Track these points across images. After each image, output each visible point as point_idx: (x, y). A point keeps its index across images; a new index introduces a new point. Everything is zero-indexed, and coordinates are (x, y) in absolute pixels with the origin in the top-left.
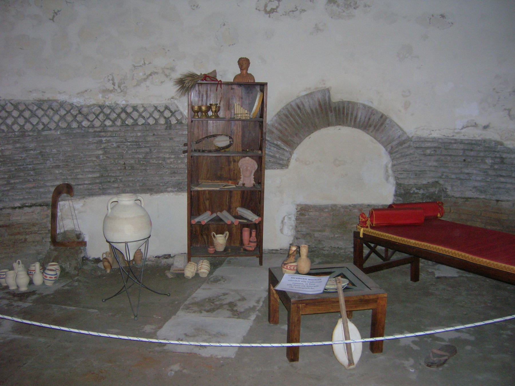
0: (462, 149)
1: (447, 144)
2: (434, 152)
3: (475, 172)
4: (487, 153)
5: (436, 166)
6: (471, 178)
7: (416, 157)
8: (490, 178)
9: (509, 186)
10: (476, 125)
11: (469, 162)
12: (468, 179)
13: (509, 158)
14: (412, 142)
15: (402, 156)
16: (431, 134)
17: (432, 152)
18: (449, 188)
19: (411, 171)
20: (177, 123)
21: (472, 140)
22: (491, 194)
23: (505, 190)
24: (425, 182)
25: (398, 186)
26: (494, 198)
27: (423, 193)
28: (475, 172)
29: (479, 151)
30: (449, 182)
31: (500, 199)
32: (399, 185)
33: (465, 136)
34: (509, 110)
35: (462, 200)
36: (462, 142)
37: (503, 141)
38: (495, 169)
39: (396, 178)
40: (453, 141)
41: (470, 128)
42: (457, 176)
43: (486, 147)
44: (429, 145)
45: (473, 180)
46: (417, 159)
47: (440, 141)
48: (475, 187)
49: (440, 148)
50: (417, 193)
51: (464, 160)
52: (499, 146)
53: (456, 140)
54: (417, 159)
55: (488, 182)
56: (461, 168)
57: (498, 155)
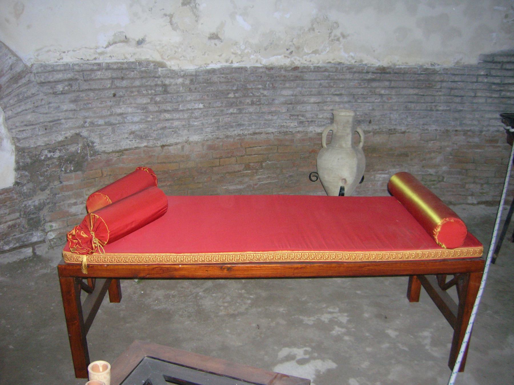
0: (110, 79)
1: (88, 73)
2: (69, 87)
3: (130, 110)
4: (144, 81)
5: (75, 110)
6: (126, 120)
7: (42, 100)
8: (151, 117)
9: (176, 123)
10: (126, 40)
11: (121, 97)
12: (122, 123)
13: (174, 85)
14: (32, 75)
15: (20, 101)
16: (62, 59)
17: (66, 88)
18: (97, 140)
19: (36, 124)
20: (234, 97)
21: (123, 63)
22: (155, 139)
23: (171, 130)
24: (61, 138)
25: (20, 153)
26: (159, 143)
27: (60, 157)
28: (130, 110)
29: (132, 79)
30: (96, 132)
31: (167, 144)
32: (20, 151)
33: (113, 58)
34: (171, 16)
35: (117, 154)
36: (108, 67)
37: (165, 61)
38: (156, 103)
39: (16, 140)
40: (95, 68)
41: (118, 45)
42: (107, 120)
43: (142, 72)
44: (59, 76)
45: (129, 123)
46: (43, 103)
47: (77, 68)
48: (132, 133)
49: (76, 79)
50: (51, 158)
51: (114, 95)
52: (160, 69)
53: (99, 64)
54: (43, 103)
55: (149, 121)
56: (111, 107)
57: (159, 83)
